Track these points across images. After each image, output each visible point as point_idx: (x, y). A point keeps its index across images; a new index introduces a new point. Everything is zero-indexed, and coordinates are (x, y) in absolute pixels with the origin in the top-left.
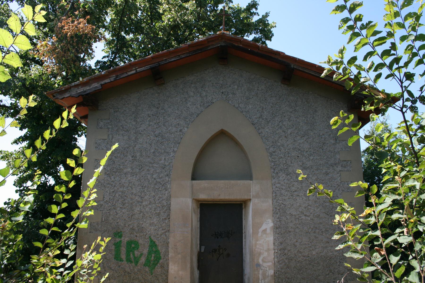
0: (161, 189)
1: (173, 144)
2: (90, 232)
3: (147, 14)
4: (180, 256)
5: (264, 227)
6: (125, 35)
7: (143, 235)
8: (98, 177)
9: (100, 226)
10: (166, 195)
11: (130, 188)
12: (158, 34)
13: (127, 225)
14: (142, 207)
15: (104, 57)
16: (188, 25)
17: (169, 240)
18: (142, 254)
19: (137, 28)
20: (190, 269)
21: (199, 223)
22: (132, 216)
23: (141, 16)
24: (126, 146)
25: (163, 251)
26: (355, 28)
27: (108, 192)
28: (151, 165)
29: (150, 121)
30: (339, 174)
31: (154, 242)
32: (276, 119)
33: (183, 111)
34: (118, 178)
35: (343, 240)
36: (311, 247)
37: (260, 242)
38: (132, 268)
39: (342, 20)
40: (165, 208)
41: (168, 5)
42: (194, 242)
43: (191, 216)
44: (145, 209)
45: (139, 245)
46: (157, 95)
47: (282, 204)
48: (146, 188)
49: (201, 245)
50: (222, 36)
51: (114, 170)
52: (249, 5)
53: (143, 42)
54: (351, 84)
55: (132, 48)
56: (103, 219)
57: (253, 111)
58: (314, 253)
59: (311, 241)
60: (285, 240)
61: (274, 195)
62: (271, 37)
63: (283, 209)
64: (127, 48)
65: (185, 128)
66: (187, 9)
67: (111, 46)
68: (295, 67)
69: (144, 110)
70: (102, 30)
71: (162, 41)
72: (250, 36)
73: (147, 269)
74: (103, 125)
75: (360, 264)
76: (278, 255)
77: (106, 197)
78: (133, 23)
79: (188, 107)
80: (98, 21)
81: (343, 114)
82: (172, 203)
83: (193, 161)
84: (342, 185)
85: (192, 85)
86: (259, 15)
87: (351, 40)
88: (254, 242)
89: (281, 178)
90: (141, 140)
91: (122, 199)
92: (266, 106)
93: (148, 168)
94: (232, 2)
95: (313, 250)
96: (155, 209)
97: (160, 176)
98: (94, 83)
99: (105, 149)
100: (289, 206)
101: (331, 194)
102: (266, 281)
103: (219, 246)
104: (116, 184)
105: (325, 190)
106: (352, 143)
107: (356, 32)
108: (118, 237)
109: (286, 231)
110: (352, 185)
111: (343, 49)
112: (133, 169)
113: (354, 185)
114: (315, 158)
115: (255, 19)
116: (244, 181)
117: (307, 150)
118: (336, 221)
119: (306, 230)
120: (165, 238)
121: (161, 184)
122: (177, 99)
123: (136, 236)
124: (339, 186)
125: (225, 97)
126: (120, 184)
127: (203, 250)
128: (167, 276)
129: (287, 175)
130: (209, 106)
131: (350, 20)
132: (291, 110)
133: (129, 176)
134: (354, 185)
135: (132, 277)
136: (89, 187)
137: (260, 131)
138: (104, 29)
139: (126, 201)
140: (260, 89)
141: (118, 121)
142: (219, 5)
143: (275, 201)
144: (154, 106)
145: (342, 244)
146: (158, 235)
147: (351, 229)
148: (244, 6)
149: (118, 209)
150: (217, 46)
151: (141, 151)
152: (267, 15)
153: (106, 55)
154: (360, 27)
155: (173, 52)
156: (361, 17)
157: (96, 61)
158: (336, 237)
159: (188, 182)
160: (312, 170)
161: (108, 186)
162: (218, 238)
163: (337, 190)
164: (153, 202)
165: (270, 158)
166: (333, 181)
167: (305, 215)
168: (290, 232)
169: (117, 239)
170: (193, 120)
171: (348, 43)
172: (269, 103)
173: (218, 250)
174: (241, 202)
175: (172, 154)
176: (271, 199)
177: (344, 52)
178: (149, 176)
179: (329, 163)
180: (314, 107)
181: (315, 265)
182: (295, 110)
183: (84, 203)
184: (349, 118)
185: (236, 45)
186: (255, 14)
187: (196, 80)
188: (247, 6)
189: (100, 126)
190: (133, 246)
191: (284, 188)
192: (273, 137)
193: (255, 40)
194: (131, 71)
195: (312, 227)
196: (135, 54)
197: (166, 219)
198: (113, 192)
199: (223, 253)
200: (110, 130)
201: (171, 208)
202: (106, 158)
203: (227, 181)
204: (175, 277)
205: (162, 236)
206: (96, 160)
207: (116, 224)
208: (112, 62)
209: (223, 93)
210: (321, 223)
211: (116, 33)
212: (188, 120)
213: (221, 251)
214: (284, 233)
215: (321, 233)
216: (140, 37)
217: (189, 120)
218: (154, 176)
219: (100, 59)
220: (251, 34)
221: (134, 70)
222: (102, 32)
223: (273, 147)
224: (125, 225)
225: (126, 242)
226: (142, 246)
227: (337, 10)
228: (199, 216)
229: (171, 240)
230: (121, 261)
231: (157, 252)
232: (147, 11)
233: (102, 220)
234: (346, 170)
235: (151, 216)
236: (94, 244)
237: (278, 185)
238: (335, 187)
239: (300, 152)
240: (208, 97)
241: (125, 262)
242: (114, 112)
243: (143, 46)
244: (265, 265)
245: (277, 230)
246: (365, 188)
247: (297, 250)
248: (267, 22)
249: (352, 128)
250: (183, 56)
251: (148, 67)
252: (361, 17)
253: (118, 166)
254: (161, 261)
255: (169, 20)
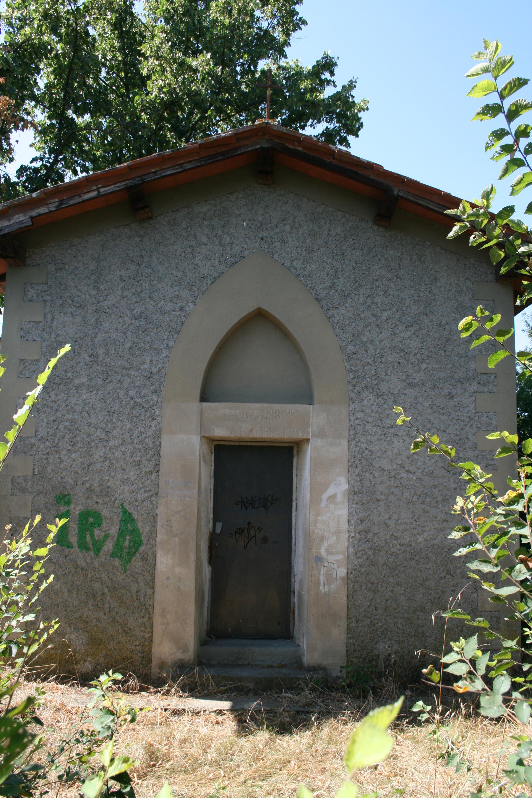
0: (142, 417)
1: (167, 333)
2: (12, 495)
3: (118, 75)
4: (177, 539)
5: (331, 491)
6: (74, 116)
7: (110, 501)
8: (33, 406)
9: (30, 483)
10: (153, 428)
11: (85, 414)
12: (139, 118)
13: (79, 483)
14: (108, 449)
15: (34, 160)
16: (197, 102)
17: (158, 511)
18: (107, 536)
19: (98, 104)
20: (195, 563)
21: (212, 481)
22: (89, 466)
23: (105, 78)
24: (78, 335)
25: (147, 529)
26: (516, 150)
27: (45, 420)
28: (125, 372)
29: (123, 289)
30: (473, 399)
31: (130, 515)
32: (362, 291)
33: (187, 271)
34: (63, 394)
35: (470, 540)
36: (415, 528)
37: (324, 518)
38: (89, 560)
39: (493, 132)
40: (151, 453)
41: (157, 60)
42: (203, 515)
43: (198, 468)
44: (113, 453)
45: (101, 519)
46: (137, 239)
47: (366, 449)
48: (115, 415)
49: (215, 520)
50: (265, 129)
51: (56, 381)
52: (318, 65)
53: (110, 131)
54: (500, 255)
55: (88, 142)
56: (36, 470)
57: (318, 275)
58: (420, 539)
59: (416, 517)
60: (368, 515)
61: (352, 432)
62: (359, 129)
63: (366, 459)
64: (79, 142)
65: (190, 304)
66: (196, 71)
67: (48, 138)
68: (401, 194)
69: (113, 267)
70: (29, 105)
71: (147, 130)
72: (318, 125)
73: (117, 562)
74: (35, 295)
75: (495, 579)
76: (356, 542)
77: (40, 429)
78: (90, 92)
79: (197, 265)
80: (23, 87)
81: (482, 312)
82: (163, 443)
83: (203, 366)
84: (476, 418)
85: (206, 223)
86: (335, 86)
87: (506, 172)
88: (312, 518)
89: (365, 402)
90: (106, 325)
91: (71, 434)
92: (344, 266)
93: (119, 377)
94: (286, 57)
95: (419, 534)
96: (132, 454)
97: (142, 394)
98: (18, 213)
99: (39, 340)
100: (379, 455)
101: (453, 453)
102: (332, 586)
103: (249, 523)
104: (59, 406)
105: (443, 446)
106: (495, 363)
107: (517, 159)
108: (63, 503)
109: (371, 499)
110: (490, 437)
111: (489, 190)
112: (91, 379)
113: (494, 436)
114: (430, 366)
115: (329, 92)
116: (299, 405)
117: (416, 351)
118: (457, 507)
119: (409, 497)
120: (150, 507)
121: (143, 408)
122: (175, 247)
123: (97, 503)
124: (471, 419)
125: (266, 246)
126: (67, 406)
127: (218, 531)
128: (153, 575)
129: (378, 396)
130: (236, 262)
131: (508, 133)
132: (390, 275)
133: (84, 392)
134: (494, 436)
135: (90, 576)
136: (16, 424)
137: (330, 313)
138: (33, 103)
139: (79, 439)
140: (333, 233)
141: (63, 287)
142: (260, 62)
143: (353, 443)
144: (133, 261)
145: (465, 547)
146: (137, 501)
147: (482, 522)
148: (307, 64)
149: (64, 452)
150: (254, 148)
151: (108, 344)
152: (351, 86)
153: (38, 154)
154: (525, 149)
155: (169, 158)
156: (528, 131)
157: (18, 167)
158: (456, 535)
159: (194, 406)
160: (424, 389)
161: (45, 409)
162: (246, 508)
163: (468, 427)
164: (129, 440)
165: (346, 364)
166: (461, 409)
167: (407, 471)
168: (378, 500)
169: (62, 508)
170: (205, 288)
171: (501, 178)
172: (349, 260)
173: (246, 531)
174: (291, 445)
175: (165, 353)
176: (346, 441)
177: (491, 196)
178: (121, 393)
179: (456, 376)
180: (433, 270)
181: (421, 560)
182: (397, 276)
183: (7, 451)
184: (491, 320)
185: (291, 147)
186: (328, 82)
187: (212, 212)
188: (314, 67)
189: (29, 297)
190: (91, 520)
191: (370, 420)
192: (354, 324)
193: (328, 134)
194: (89, 192)
195: (419, 493)
196: (94, 155)
197: (151, 472)
198: (54, 421)
199: (255, 536)
200: (49, 304)
201: (162, 452)
202: (47, 372)
203: (266, 405)
204: (168, 578)
205: (145, 503)
206: (22, 360)
207: (59, 479)
208: (51, 169)
209: (262, 239)
210: (435, 487)
211: (57, 111)
212: (195, 289)
213: (252, 532)
214: (368, 503)
215: (435, 505)
216: (105, 122)
217: (198, 289)
218: (131, 393)
219: (27, 163)
220: (319, 122)
221: (94, 190)
222: (30, 109)
223: (353, 343)
224: (76, 482)
225: (77, 513)
226: (108, 521)
227: (486, 114)
228: (213, 468)
229: (161, 511)
230: (68, 547)
231: (135, 532)
232: (119, 71)
233: (34, 472)
234: (486, 390)
235: (124, 467)
236: (27, 526)
237: (360, 415)
238: (464, 421)
239: (402, 354)
240: (234, 246)
241: (76, 550)
242: (56, 270)
243: (109, 139)
244: (331, 558)
245: (356, 497)
246: (512, 443)
247: (391, 533)
248: (350, 100)
249: (497, 338)
250: (189, 166)
251: (121, 185)
252: (528, 131)
253: (63, 373)
254: (142, 549)
255: (160, 89)
